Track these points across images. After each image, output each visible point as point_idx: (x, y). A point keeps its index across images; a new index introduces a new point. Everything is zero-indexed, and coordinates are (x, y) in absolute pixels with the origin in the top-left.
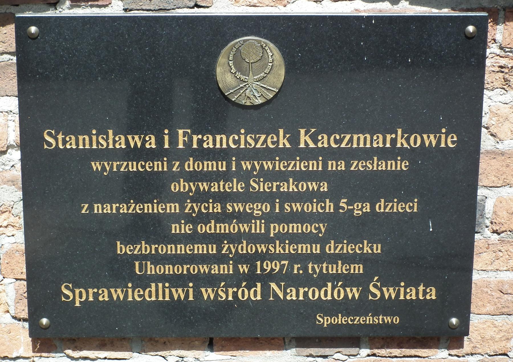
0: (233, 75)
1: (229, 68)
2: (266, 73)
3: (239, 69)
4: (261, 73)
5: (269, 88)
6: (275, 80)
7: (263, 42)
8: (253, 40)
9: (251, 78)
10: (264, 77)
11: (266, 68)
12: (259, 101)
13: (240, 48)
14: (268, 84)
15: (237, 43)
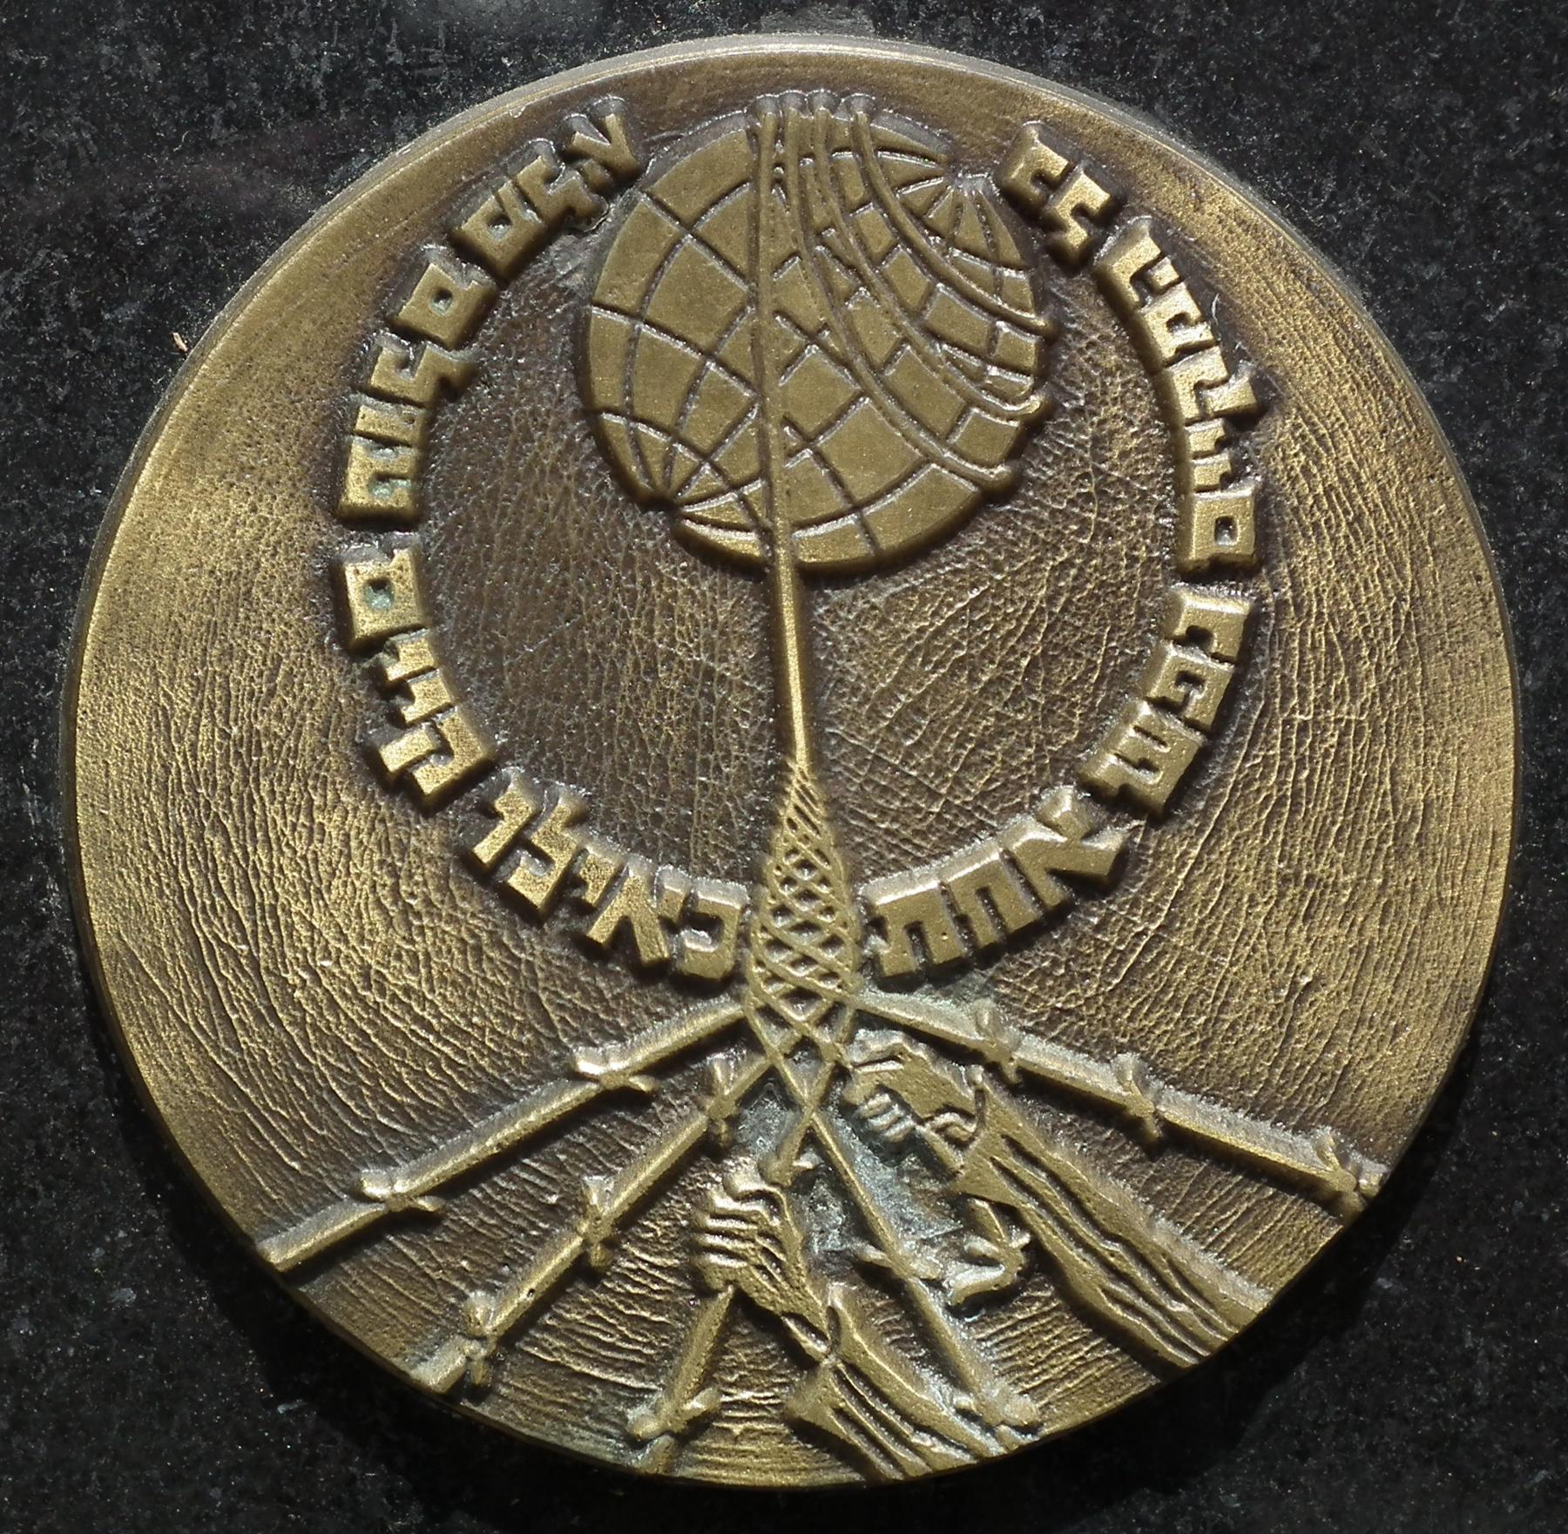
0: (429, 838)
1: (327, 680)
2: (1116, 802)
3: (550, 709)
4: (1011, 796)
5: (1185, 1111)
6: (1319, 949)
7: (1058, 133)
8: (841, 80)
9: (806, 910)
10: (1087, 887)
11: (1123, 678)
12: (981, 1404)
13: (567, 261)
14: (1165, 1028)
15: (506, 146)
